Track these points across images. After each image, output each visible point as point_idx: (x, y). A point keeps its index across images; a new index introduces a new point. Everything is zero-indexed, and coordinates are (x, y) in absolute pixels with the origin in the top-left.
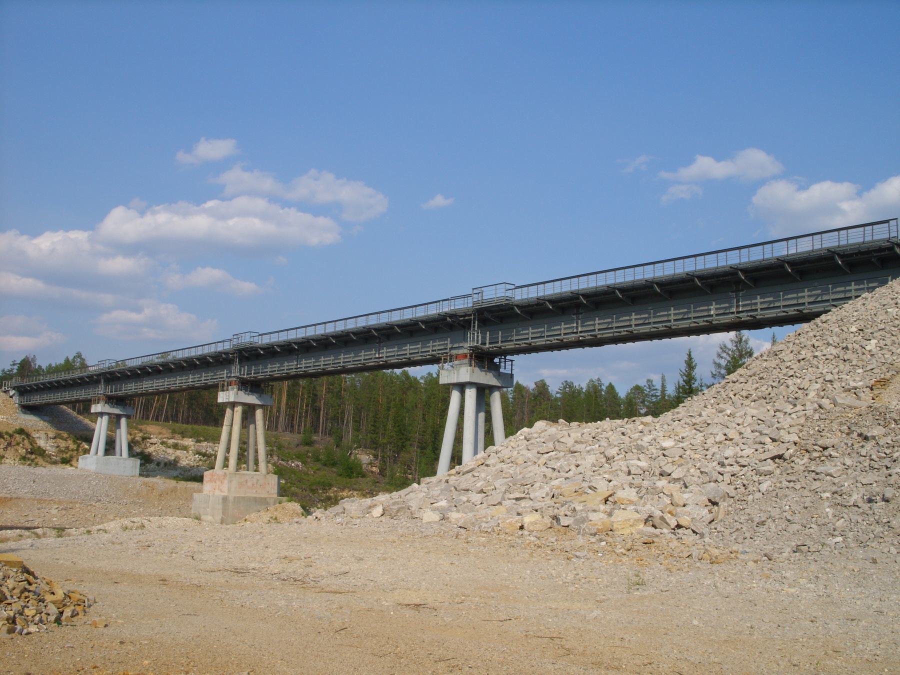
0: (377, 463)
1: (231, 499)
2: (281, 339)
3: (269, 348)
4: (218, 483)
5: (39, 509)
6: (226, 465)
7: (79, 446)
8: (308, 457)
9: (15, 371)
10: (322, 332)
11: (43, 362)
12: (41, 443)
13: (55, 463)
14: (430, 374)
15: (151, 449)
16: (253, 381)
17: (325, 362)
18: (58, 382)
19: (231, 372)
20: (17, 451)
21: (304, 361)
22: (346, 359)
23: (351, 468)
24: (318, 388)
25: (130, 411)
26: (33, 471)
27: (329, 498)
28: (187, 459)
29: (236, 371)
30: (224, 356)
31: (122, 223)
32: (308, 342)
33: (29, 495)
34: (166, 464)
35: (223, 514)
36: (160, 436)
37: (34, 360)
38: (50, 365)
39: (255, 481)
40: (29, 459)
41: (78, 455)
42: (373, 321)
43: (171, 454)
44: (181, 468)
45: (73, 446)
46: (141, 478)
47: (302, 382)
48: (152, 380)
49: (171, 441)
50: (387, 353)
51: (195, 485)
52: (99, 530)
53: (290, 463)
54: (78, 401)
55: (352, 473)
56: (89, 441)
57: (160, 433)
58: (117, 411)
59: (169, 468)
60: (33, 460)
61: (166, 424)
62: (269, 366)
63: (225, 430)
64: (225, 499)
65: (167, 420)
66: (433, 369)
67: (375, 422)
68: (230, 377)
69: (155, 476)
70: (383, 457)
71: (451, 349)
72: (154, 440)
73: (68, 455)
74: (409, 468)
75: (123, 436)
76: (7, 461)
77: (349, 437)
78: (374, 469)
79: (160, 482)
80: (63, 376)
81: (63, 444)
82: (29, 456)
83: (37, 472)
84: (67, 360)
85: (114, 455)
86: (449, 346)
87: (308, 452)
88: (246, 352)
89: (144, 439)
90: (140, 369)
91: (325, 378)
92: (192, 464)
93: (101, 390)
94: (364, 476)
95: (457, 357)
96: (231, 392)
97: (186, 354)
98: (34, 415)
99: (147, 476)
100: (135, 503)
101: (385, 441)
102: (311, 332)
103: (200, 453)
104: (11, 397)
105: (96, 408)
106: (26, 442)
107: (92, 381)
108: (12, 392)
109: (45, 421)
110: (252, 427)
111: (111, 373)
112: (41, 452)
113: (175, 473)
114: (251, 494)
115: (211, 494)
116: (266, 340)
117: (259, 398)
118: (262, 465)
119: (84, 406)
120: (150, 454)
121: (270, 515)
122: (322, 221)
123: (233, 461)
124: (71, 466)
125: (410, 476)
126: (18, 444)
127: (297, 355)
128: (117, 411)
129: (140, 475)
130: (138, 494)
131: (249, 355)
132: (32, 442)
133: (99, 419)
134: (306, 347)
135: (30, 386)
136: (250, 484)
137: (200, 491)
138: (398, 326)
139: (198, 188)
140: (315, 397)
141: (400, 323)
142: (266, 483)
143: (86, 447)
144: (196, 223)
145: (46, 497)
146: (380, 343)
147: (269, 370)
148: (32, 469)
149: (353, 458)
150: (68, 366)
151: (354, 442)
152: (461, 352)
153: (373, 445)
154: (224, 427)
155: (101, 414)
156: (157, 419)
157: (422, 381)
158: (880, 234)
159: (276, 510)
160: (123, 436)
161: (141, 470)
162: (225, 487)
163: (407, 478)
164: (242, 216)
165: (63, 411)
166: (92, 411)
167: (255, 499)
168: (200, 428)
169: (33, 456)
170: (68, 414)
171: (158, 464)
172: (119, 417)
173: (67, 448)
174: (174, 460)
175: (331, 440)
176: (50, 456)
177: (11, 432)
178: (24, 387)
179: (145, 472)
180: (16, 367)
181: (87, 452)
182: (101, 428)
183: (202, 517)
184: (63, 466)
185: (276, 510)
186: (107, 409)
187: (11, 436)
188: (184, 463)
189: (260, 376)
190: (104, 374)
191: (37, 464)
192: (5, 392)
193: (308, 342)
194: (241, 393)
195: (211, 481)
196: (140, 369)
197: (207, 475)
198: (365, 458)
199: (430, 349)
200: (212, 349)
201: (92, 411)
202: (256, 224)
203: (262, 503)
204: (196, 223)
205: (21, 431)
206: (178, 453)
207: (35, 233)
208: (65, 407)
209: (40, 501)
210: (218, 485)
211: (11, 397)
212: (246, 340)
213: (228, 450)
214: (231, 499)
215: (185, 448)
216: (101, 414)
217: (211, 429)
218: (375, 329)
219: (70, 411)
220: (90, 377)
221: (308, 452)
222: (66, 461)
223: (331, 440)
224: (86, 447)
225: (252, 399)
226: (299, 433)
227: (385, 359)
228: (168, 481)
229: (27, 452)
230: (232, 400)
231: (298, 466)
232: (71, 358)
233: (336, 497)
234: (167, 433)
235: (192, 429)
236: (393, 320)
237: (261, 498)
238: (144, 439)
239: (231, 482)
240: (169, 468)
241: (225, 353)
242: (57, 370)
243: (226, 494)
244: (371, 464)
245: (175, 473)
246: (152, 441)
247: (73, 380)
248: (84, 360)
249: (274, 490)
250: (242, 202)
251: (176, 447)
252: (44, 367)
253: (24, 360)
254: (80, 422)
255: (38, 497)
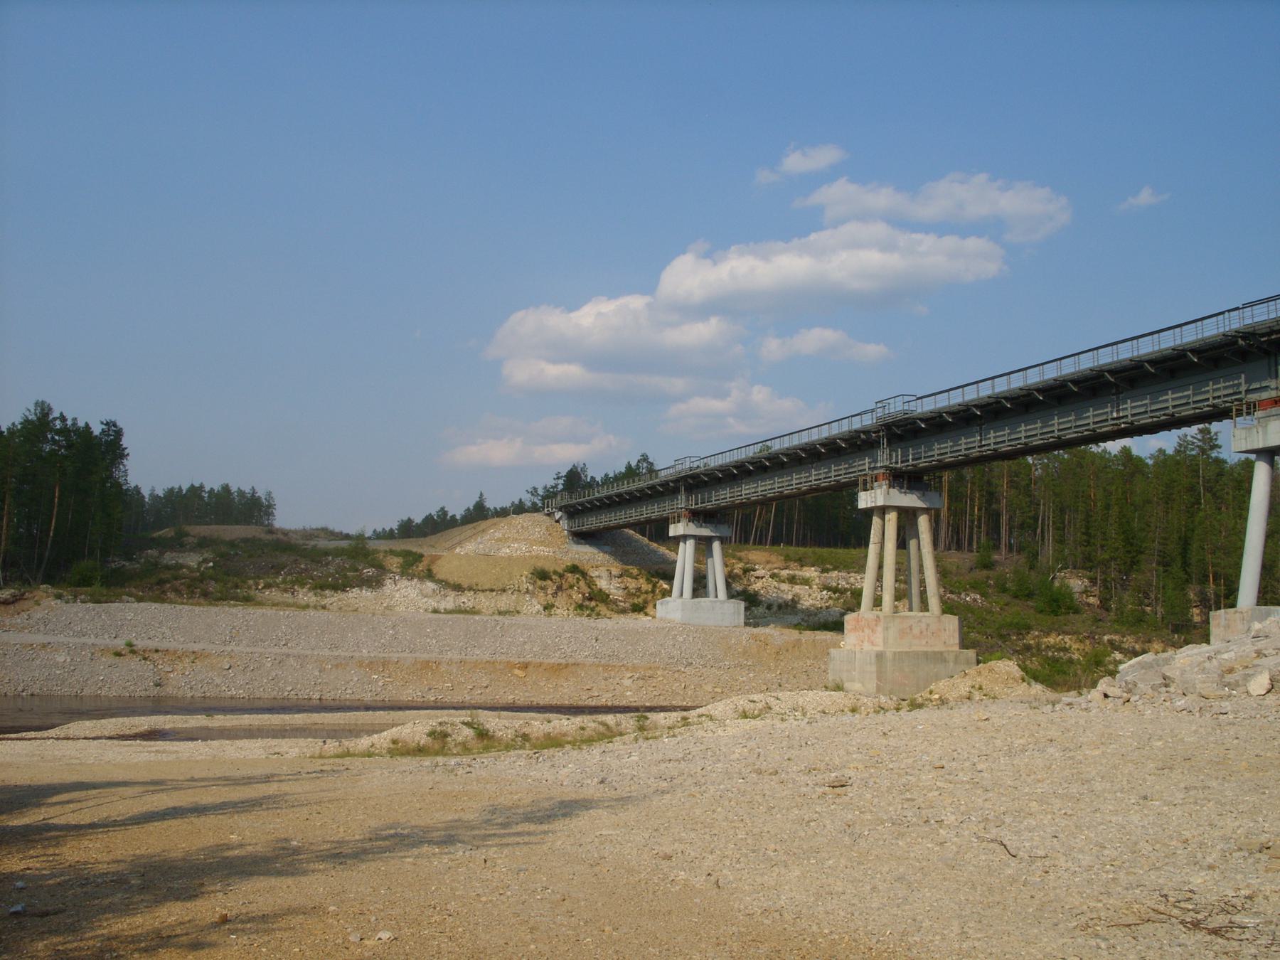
0: (1096, 590)
1: (889, 655)
2: (953, 402)
3: (933, 418)
4: (867, 631)
5: (606, 679)
6: (877, 602)
7: (654, 586)
8: (989, 586)
9: (560, 487)
10: (959, 400)
11: (596, 472)
12: (603, 584)
13: (623, 611)
14: (1161, 451)
15: (757, 586)
16: (909, 472)
17: (997, 438)
18: (619, 495)
19: (876, 461)
20: (570, 596)
21: (992, 434)
22: (1027, 432)
23: (1056, 601)
24: (994, 481)
25: (726, 531)
26: (593, 625)
27: (1028, 648)
28: (811, 598)
29: (884, 458)
30: (863, 436)
31: (688, 276)
32: (941, 416)
33: (590, 660)
34: (780, 607)
35: (879, 679)
36: (768, 566)
37: (584, 470)
38: (606, 475)
39: (923, 626)
40: (587, 608)
41: (654, 600)
42: (1001, 387)
43: (787, 592)
44: (803, 611)
45: (646, 587)
46: (748, 629)
47: (968, 473)
48: (755, 482)
49: (785, 573)
50: (1092, 417)
51: (828, 636)
52: (700, 716)
53: (963, 596)
54: (649, 521)
55: (1059, 607)
56: (669, 577)
57: (768, 562)
58: (705, 532)
59: (785, 611)
60: (593, 609)
61: (775, 548)
62: (937, 446)
63: (873, 549)
64: (880, 656)
65: (775, 542)
66: (1125, 442)
67: (1088, 528)
68: (875, 468)
69: (767, 625)
70: (1104, 581)
71: (1248, 391)
72: (760, 572)
73: (640, 600)
74: (1147, 596)
75: (717, 568)
76: (558, 611)
77: (1048, 551)
78: (1091, 600)
79: (775, 634)
80: (626, 487)
81: (632, 584)
82: (587, 603)
83: (600, 626)
84: (629, 467)
85: (706, 595)
86: (1243, 388)
87: (988, 578)
88: (898, 427)
89: (746, 571)
90: (735, 467)
91: (1006, 463)
92: (818, 604)
93: (681, 502)
94: (1077, 612)
95: (1262, 405)
96: (879, 491)
97: (787, 443)
98: (590, 544)
99: (756, 625)
100: (740, 665)
101: (1107, 557)
102: (1106, 358)
103: (829, 589)
104: (557, 521)
105: (675, 530)
106: (582, 583)
107: (668, 489)
108: (558, 515)
109: (605, 552)
110: (913, 544)
111: (695, 477)
112: (603, 597)
113: (796, 619)
114: (920, 646)
115: (858, 649)
116: (928, 406)
117: (921, 498)
118: (934, 602)
119: (658, 530)
120: (756, 594)
121: (970, 683)
122: (972, 243)
123: (887, 598)
124: (646, 614)
125: (1148, 609)
126: (571, 587)
127: (980, 425)
128: (705, 532)
129: (746, 624)
130: (745, 652)
131: (902, 431)
132: (590, 583)
133: (681, 544)
134: (995, 411)
135: (581, 504)
136: (916, 631)
137: (836, 645)
138: (1150, 362)
139: (788, 221)
140: (991, 497)
141: (1153, 356)
142: (944, 631)
143: (666, 586)
144: (787, 266)
145: (615, 662)
146: (1117, 393)
147: (936, 452)
148: (591, 622)
149: (1057, 584)
150: (631, 473)
151: (1057, 560)
152: (1265, 395)
153: (1086, 563)
154: (871, 546)
155: (685, 538)
156: (760, 543)
157: (1150, 462)
158: (1261, 316)
159: (980, 673)
160: (717, 568)
161: (746, 617)
162: (879, 638)
163: (1144, 611)
164: (854, 251)
165: (629, 540)
166: (671, 534)
167: (926, 653)
168: (825, 551)
169: (593, 604)
170: (637, 541)
171: (769, 607)
172: (708, 541)
173: (639, 589)
174: (793, 600)
175: (1022, 559)
176: (615, 602)
177: (560, 571)
178: (573, 506)
179: (752, 620)
180: (561, 481)
181: (666, 593)
182: (685, 557)
183: (847, 685)
184: (635, 615)
185: (980, 673)
186: (693, 529)
187: (561, 576)
188: (806, 603)
189: (922, 464)
190: (684, 478)
191: (598, 614)
192: (548, 515)
193: (1029, 395)
194: (894, 492)
195: (855, 629)
196: (735, 467)
197: (849, 619)
198: (1077, 584)
199: (1055, 428)
200: (845, 427)
201: (671, 534)
202: (873, 258)
203: (939, 657)
204: (787, 266)
205: (574, 569)
206: (797, 589)
207: (573, 305)
208: (631, 532)
209: (606, 667)
210: (866, 638)
211: (557, 521)
212: (897, 408)
213: (879, 578)
214: (889, 655)
215: (806, 582)
216: (685, 538)
217: (854, 552)
218: (1110, 372)
219: (638, 536)
220: (665, 484)
221: (988, 578)
222: (638, 609)
223: (1022, 559)
224: (666, 586)
225: (911, 500)
226: (971, 551)
227: (1130, 419)
228: (786, 631)
229: (584, 598)
230: (880, 503)
231: (975, 600)
232: (634, 464)
233: (1038, 645)
234: (777, 560)
235: (814, 553)
236: (1101, 362)
237: (935, 653)
238: (746, 571)
239: (887, 629)
240: (785, 611)
241: (864, 432)
242: (618, 478)
243: (880, 648)
244: (1085, 592)
245: (796, 619)
246: (758, 573)
247: (641, 491)
248: (652, 464)
249: (955, 640)
250: (851, 228)
251: (792, 580)
252: (598, 479)
253: (571, 471)
254: (655, 552)
255: (603, 662)
